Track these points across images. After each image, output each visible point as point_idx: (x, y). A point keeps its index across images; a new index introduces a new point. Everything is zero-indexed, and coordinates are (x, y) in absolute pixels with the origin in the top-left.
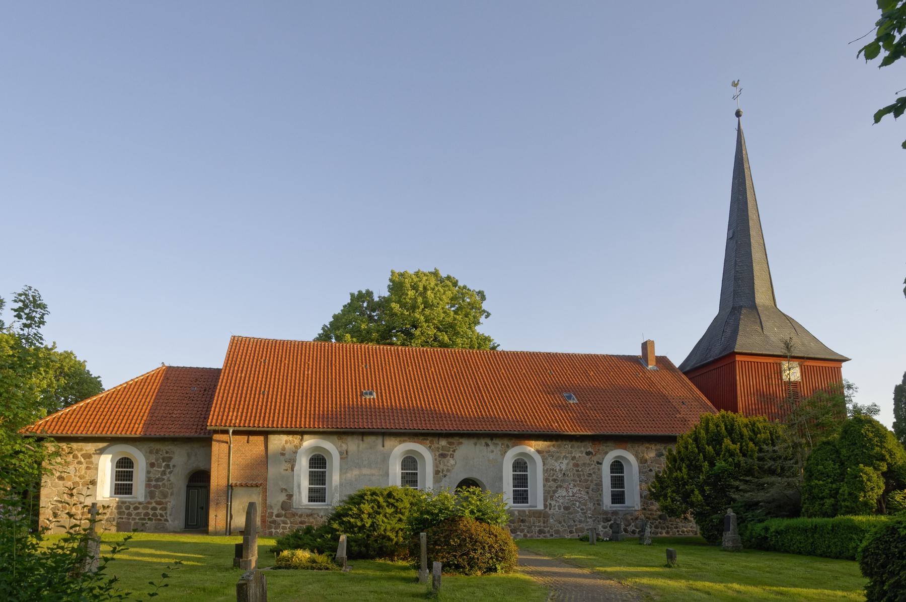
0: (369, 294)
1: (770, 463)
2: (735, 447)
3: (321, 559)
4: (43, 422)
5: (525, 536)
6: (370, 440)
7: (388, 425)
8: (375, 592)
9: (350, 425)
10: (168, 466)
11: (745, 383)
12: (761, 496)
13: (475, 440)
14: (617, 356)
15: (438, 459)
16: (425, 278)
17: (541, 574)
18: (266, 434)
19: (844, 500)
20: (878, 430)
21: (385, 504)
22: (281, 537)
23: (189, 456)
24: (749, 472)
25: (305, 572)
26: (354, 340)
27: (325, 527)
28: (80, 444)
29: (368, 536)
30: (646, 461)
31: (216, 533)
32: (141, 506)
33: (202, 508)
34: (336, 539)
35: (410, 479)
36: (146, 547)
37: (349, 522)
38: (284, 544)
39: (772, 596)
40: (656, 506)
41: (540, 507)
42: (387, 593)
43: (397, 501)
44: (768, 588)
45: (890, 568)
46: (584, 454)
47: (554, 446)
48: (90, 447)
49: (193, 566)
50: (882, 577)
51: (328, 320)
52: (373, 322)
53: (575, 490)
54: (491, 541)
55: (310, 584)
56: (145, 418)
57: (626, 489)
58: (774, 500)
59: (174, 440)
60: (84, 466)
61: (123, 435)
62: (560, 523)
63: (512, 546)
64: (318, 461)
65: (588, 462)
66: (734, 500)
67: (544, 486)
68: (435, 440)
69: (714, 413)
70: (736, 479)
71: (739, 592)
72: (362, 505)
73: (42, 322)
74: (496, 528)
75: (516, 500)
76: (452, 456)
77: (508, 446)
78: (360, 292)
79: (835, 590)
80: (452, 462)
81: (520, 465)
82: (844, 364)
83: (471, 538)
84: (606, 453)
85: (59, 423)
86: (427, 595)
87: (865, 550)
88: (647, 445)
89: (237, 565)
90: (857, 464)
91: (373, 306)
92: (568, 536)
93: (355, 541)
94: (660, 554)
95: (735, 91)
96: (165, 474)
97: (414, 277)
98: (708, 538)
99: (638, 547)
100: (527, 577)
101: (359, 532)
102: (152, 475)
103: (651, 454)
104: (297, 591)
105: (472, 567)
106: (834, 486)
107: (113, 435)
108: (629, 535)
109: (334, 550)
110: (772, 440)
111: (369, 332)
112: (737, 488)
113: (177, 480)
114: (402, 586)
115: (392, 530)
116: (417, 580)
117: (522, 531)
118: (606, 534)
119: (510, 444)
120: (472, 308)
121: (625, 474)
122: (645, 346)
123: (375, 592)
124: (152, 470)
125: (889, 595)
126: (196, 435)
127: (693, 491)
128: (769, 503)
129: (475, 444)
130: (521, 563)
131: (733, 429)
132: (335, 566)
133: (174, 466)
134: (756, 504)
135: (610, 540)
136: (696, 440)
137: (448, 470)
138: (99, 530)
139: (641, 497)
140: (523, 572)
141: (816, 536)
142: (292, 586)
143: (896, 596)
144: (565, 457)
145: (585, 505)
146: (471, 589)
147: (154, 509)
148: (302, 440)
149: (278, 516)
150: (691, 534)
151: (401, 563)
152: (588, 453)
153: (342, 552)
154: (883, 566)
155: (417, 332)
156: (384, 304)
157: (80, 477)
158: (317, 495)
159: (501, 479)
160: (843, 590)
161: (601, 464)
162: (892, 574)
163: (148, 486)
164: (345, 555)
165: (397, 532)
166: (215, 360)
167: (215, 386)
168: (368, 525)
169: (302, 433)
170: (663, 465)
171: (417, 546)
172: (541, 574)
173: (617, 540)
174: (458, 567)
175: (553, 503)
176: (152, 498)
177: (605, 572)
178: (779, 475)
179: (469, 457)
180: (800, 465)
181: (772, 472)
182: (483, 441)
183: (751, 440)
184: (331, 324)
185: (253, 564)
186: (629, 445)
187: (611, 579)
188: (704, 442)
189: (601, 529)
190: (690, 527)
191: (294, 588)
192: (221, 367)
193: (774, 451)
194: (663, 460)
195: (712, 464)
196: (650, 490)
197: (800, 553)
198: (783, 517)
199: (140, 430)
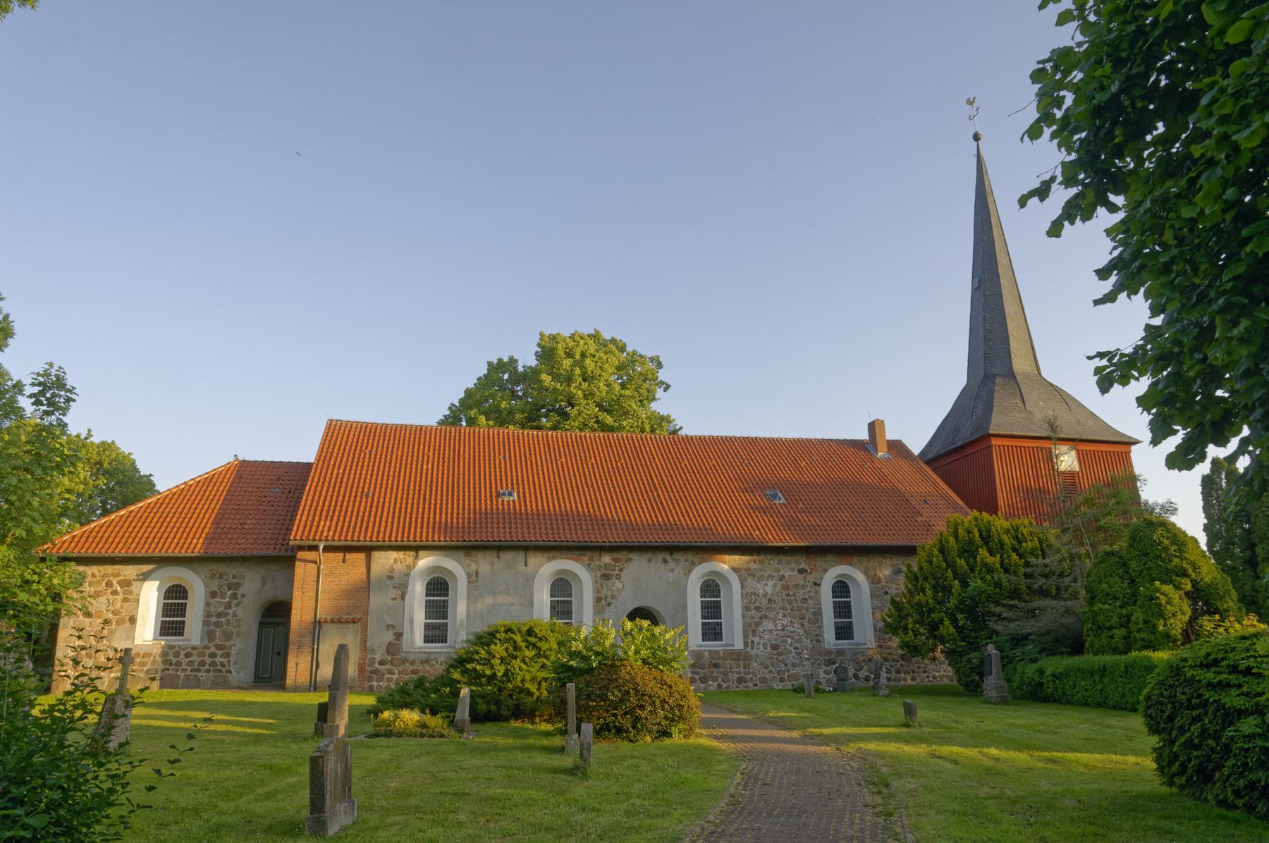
0: (513, 361)
1: (1041, 581)
2: (993, 561)
3: (435, 722)
4: (68, 535)
5: (719, 686)
6: (508, 556)
7: (533, 537)
8: (504, 767)
9: (480, 537)
10: (234, 596)
11: (1006, 475)
12: (1030, 627)
13: (649, 555)
14: (836, 441)
15: (600, 581)
16: (582, 342)
17: (733, 739)
18: (368, 550)
19: (1139, 631)
20: (1175, 535)
21: (523, 644)
22: (383, 693)
23: (264, 581)
24: (1015, 594)
25: (412, 741)
26: (491, 423)
27: (443, 677)
28: (117, 567)
29: (500, 690)
30: (879, 581)
31: (296, 689)
32: (195, 652)
33: (279, 654)
34: (455, 694)
35: (562, 609)
36: (196, 709)
37: (475, 670)
38: (388, 701)
39: (1040, 764)
40: (895, 642)
41: (739, 645)
42: (520, 769)
43: (540, 639)
44: (1037, 754)
45: (1178, 722)
46: (796, 573)
47: (755, 561)
48: (130, 571)
49: (259, 735)
50: (1170, 734)
51: (456, 396)
52: (515, 399)
53: (785, 622)
54: (663, 693)
55: (416, 757)
56: (206, 530)
57: (854, 620)
58: (1049, 632)
59: (245, 560)
60: (120, 597)
61: (177, 554)
62: (766, 667)
63: (693, 701)
64: (438, 586)
65: (801, 582)
66: (997, 633)
67: (744, 617)
68: (596, 555)
69: (966, 514)
70: (997, 603)
71: (997, 760)
72: (493, 646)
73: (65, 411)
74: (670, 677)
75: (706, 637)
76: (619, 577)
77: (693, 563)
78: (500, 360)
79: (1126, 755)
80: (619, 585)
81: (711, 588)
82: (1133, 448)
83: (636, 690)
84: (826, 570)
85: (91, 539)
86: (573, 771)
87: (1148, 698)
88: (881, 559)
89: (319, 732)
90: (1153, 580)
91: (519, 378)
92: (778, 686)
93: (483, 697)
94: (895, 708)
95: (970, 110)
96: (230, 607)
97: (568, 340)
98: (966, 686)
99: (871, 699)
100: (714, 743)
101: (488, 684)
102: (212, 609)
103: (885, 572)
104: (397, 767)
105: (638, 731)
106: (1124, 611)
107: (163, 554)
108: (861, 684)
109: (453, 709)
110: (1042, 550)
111: (511, 412)
112: (999, 615)
113: (247, 615)
114: (541, 759)
115: (533, 680)
116: (562, 750)
117: (715, 679)
118: (829, 681)
119: (696, 559)
120: (645, 380)
121: (853, 599)
122: (872, 426)
123: (504, 767)
124: (212, 601)
125: (1181, 759)
126: (275, 553)
127: (941, 621)
128: (1042, 635)
129: (650, 561)
130: (706, 724)
131: (989, 536)
132: (453, 733)
133: (243, 596)
134: (1025, 638)
135: (835, 690)
136: (942, 551)
137: (613, 597)
138: (133, 689)
139: (875, 630)
140: (710, 736)
141: (1106, 680)
142: (391, 760)
143: (1189, 760)
144: (771, 577)
145: (800, 641)
146: (631, 762)
147: (213, 655)
148: (416, 558)
149: (382, 663)
150: (946, 681)
151: (545, 727)
152: (801, 571)
153: (463, 712)
154: (1171, 719)
155: (574, 412)
156: (530, 376)
157: (114, 613)
158: (436, 634)
159: (685, 607)
160: (1137, 755)
161: (819, 585)
162: (1183, 730)
163: (206, 623)
164: (467, 717)
165: (540, 683)
166: (304, 450)
167: (304, 486)
168: (500, 674)
169: (417, 549)
170: (900, 586)
171: (564, 702)
172: (733, 739)
173: (844, 690)
174: (619, 731)
175: (756, 640)
176: (210, 641)
177: (821, 734)
178: (1055, 598)
179: (642, 578)
180: (1079, 583)
181: (1044, 593)
182: (660, 556)
183: (1015, 550)
184: (461, 401)
185: (342, 731)
186: (856, 559)
187: (827, 745)
188: (954, 553)
189: (822, 675)
190: (942, 671)
191: (395, 763)
192: (312, 460)
193: (1046, 566)
194: (902, 578)
195: (965, 584)
196: (884, 620)
197: (1086, 705)
198: (1061, 654)
199: (199, 546)
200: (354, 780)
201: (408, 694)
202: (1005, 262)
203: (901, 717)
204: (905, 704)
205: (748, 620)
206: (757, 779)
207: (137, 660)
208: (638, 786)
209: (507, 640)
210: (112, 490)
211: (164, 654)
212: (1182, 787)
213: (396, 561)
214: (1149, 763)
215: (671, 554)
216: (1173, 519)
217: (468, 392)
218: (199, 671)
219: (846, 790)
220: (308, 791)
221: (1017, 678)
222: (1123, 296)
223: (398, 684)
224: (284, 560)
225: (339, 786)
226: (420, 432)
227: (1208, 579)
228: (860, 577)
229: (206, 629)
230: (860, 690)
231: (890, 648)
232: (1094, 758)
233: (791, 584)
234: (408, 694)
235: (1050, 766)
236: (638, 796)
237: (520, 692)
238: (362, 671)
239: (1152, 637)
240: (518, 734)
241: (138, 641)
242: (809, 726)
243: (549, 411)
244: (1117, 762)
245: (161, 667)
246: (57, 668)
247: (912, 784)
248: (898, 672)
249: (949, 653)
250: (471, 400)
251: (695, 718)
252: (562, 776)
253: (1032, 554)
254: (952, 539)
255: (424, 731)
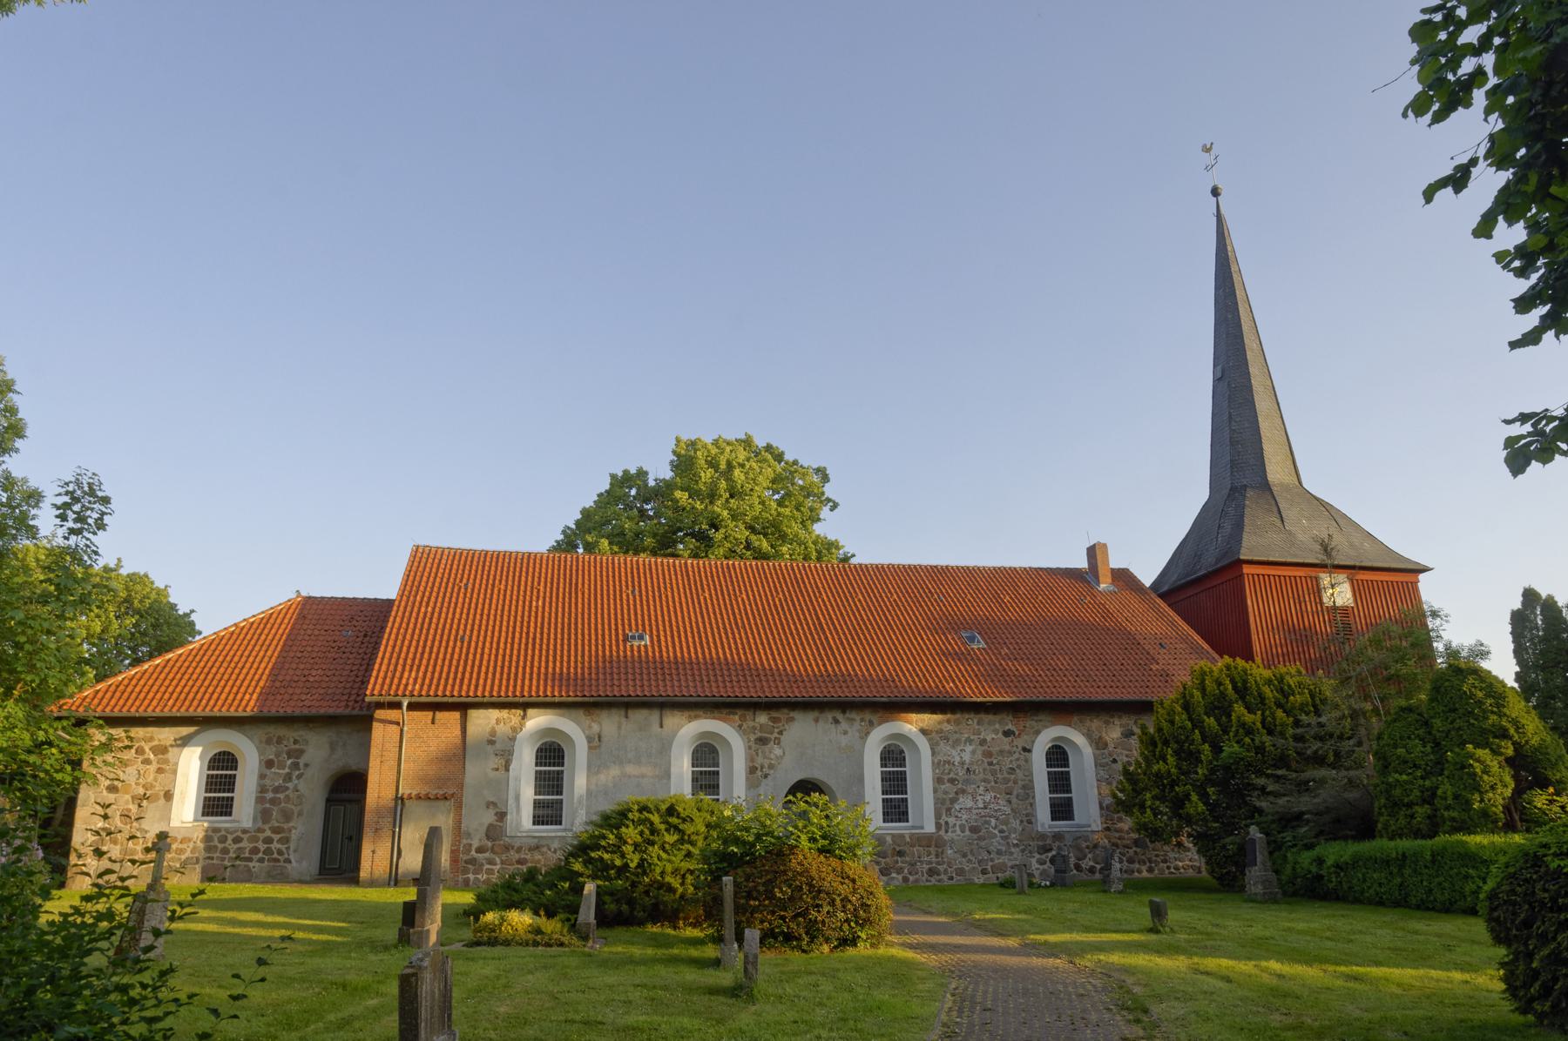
0: (642, 474)
3: (552, 926)
5: (905, 880)
6: (639, 715)
7: (670, 690)
8: (644, 986)
9: (605, 691)
10: (296, 766)
11: (1262, 611)
12: (1304, 803)
13: (816, 714)
16: (728, 449)
17: (933, 948)
18: (463, 707)
19: (1448, 808)
21: (663, 827)
23: (333, 747)
24: (1282, 761)
25: (522, 951)
27: (560, 868)
29: (634, 884)
31: (373, 883)
32: (245, 836)
33: (350, 838)
34: (578, 890)
35: (706, 782)
36: (249, 909)
37: (601, 859)
38: (487, 900)
39: (1340, 983)
40: (1127, 823)
41: (930, 828)
42: (665, 988)
43: (684, 820)
44: (1331, 968)
47: (948, 721)
48: (166, 735)
49: (328, 942)
50: (1526, 945)
51: (571, 518)
52: (647, 520)
53: (987, 798)
54: (844, 889)
56: (262, 684)
57: (1075, 795)
58: (1328, 810)
60: (153, 768)
61: (224, 713)
62: (964, 856)
63: (882, 899)
64: (551, 754)
65: (1007, 747)
66: (1260, 811)
67: (935, 791)
68: (749, 714)
69: (1214, 661)
70: (1259, 773)
71: (1280, 976)
72: (623, 829)
74: (852, 867)
75: (888, 817)
76: (778, 742)
77: (871, 723)
78: (626, 472)
79: (1448, 970)
80: (778, 751)
81: (893, 756)
82: (1421, 577)
83: (811, 886)
84: (1038, 733)
89: (404, 939)
90: (1463, 744)
91: (648, 495)
92: (979, 879)
95: (1207, 159)
98: (1220, 879)
99: (1101, 897)
100: (910, 954)
101: (618, 877)
102: (267, 782)
103: (1114, 733)
107: (207, 713)
108: (1084, 876)
109: (574, 909)
110: (1315, 706)
111: (638, 535)
112: (1263, 789)
113: (311, 790)
114: (691, 975)
115: (675, 872)
116: (716, 963)
118: (1043, 873)
119: (875, 718)
121: (1072, 769)
122: (1092, 552)
123: (644, 986)
124: (268, 772)
125: (1542, 978)
126: (348, 711)
127: (1187, 796)
129: (817, 720)
130: (899, 929)
131: (1246, 689)
132: (575, 940)
133: (306, 765)
134: (1298, 817)
135: (1053, 885)
136: (1187, 707)
137: (771, 767)
139: (1101, 808)
141: (1407, 872)
142: (498, 977)
143: (1555, 979)
145: (1006, 823)
147: (268, 841)
148: (524, 717)
149: (479, 850)
151: (691, 932)
152: (1007, 734)
153: (587, 914)
154: (1527, 924)
156: (662, 492)
158: (548, 813)
159: (861, 780)
160: (1462, 970)
161: (1029, 751)
162: (1544, 939)
163: (260, 800)
164: (592, 919)
165: (683, 876)
166: (387, 587)
167: (383, 629)
168: (633, 865)
169: (525, 706)
170: (1133, 752)
171: (718, 901)
172: (933, 948)
174: (789, 938)
177: (1046, 943)
178: (1333, 766)
179: (806, 743)
180: (1365, 747)
181: (1319, 760)
182: (829, 715)
183: (1279, 705)
184: (578, 523)
185: (433, 938)
187: (1057, 957)
188: (1201, 710)
189: (1035, 865)
190: (1188, 860)
191: (503, 981)
194: (1134, 742)
195: (1217, 749)
196: (1115, 796)
198: (1345, 838)
199: (252, 703)
200: (454, 1003)
201: (516, 891)
202: (1255, 346)
203: (1148, 923)
204: (1151, 902)
205: (940, 795)
206: (973, 1003)
207: (174, 846)
208: (820, 1012)
209: (642, 822)
210: (144, 634)
211: (207, 838)
212: (1541, 1016)
213: (498, 722)
214: (1490, 982)
215: (844, 712)
216: (1485, 665)
217: (585, 512)
218: (250, 860)
219: (1094, 1017)
220: (396, 1016)
221: (1288, 870)
222: (1549, 335)
223: (502, 877)
224: (357, 720)
225: (437, 1012)
226: (526, 561)
227: (1535, 741)
228: (1078, 738)
229: (260, 807)
230: (1085, 885)
231: (1120, 831)
232: (1407, 974)
233: (995, 750)
234: (516, 891)
235: (1351, 984)
236: (823, 1025)
237: (659, 888)
238: (454, 860)
239: (1465, 817)
240: (658, 941)
241: (175, 823)
242: (1028, 932)
243: (686, 535)
244: (1438, 981)
245: (203, 854)
246: (73, 859)
247: (1179, 1009)
248: (1131, 861)
249: (1198, 838)
250: (590, 523)
251: (885, 922)
252: (722, 999)
253: (1301, 709)
254: (1197, 694)
255: (539, 938)
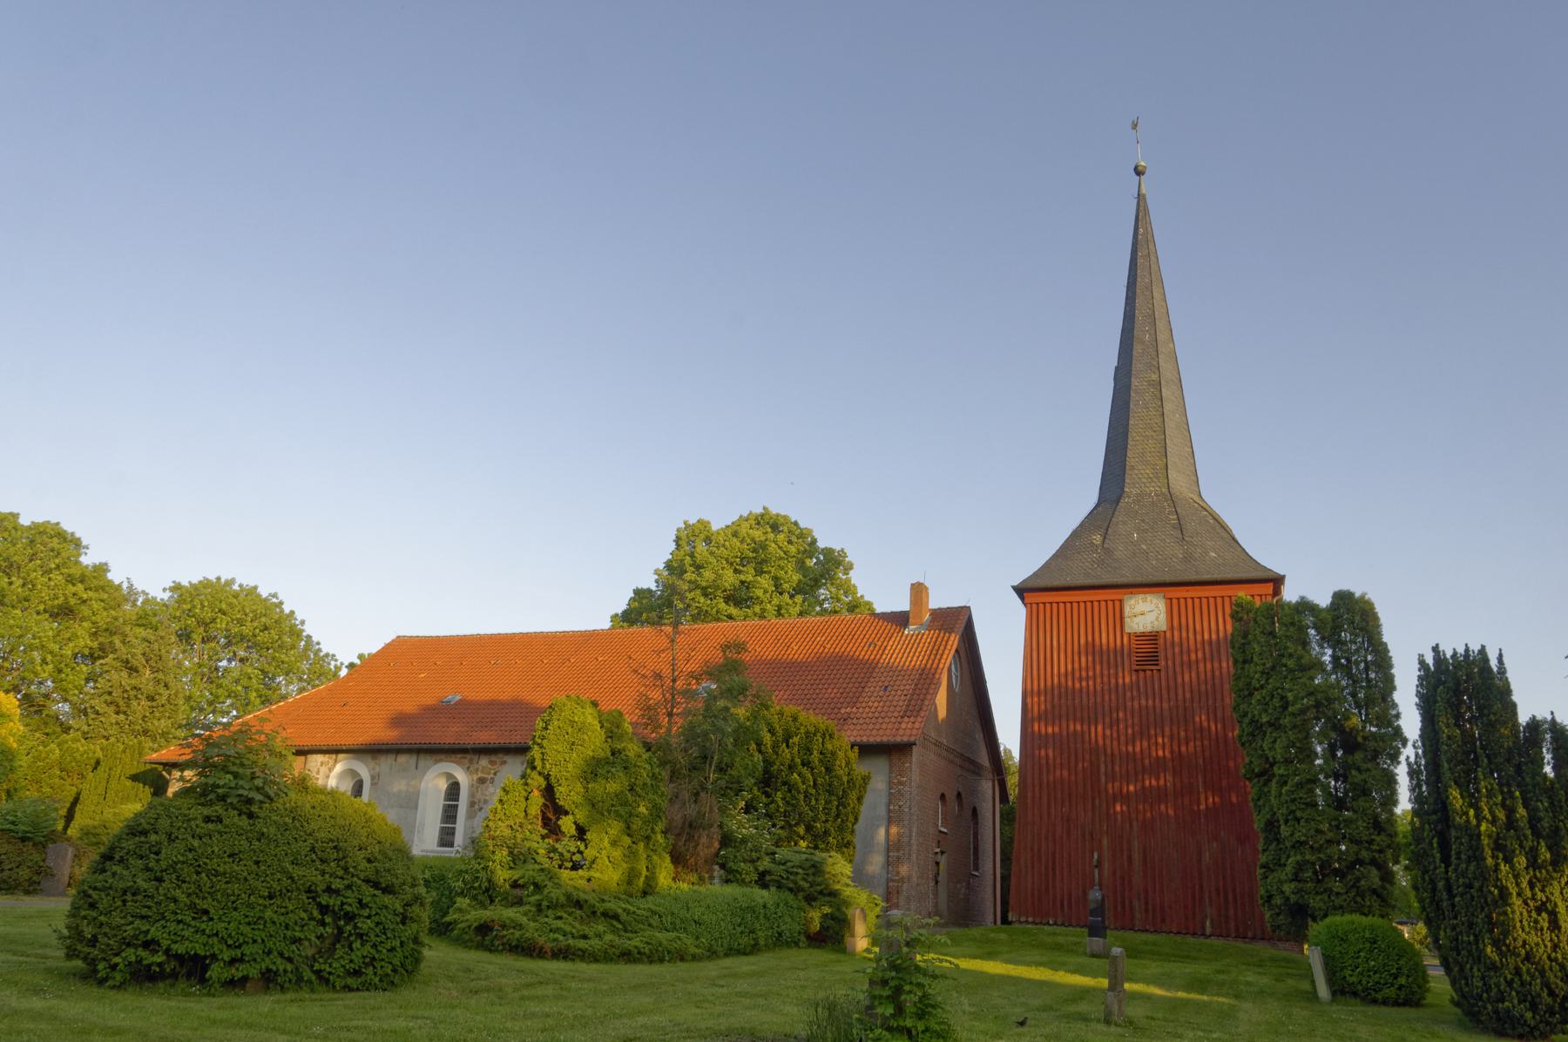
0: (1277, 581)
80: (491, 790)
158: (446, 838)
169: (337, 751)
